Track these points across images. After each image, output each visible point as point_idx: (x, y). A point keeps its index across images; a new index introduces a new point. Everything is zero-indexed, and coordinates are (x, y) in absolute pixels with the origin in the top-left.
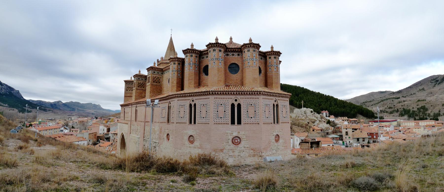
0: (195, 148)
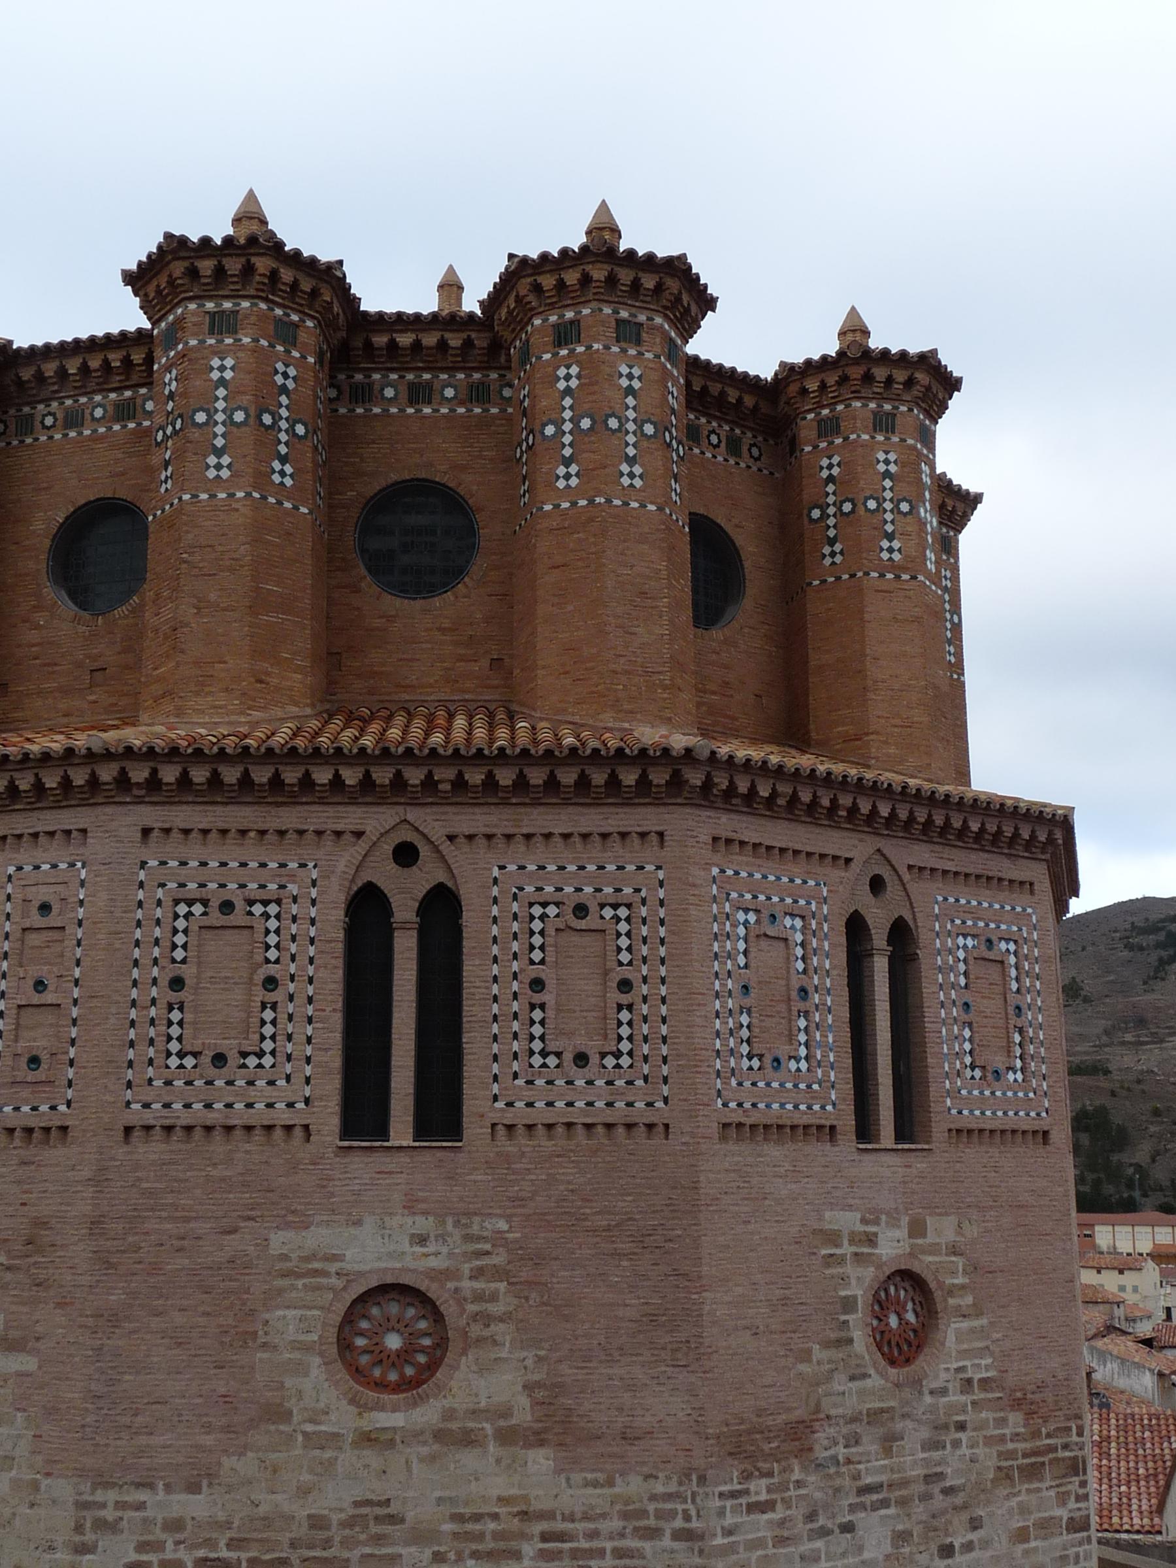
0: (455, 1437)
